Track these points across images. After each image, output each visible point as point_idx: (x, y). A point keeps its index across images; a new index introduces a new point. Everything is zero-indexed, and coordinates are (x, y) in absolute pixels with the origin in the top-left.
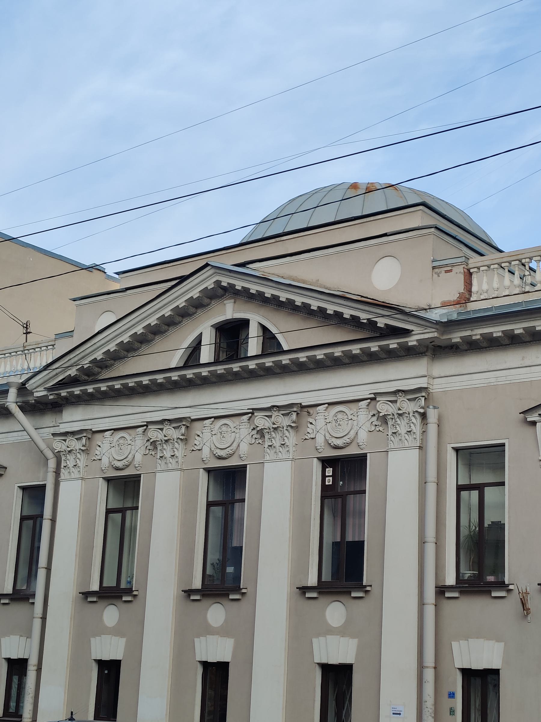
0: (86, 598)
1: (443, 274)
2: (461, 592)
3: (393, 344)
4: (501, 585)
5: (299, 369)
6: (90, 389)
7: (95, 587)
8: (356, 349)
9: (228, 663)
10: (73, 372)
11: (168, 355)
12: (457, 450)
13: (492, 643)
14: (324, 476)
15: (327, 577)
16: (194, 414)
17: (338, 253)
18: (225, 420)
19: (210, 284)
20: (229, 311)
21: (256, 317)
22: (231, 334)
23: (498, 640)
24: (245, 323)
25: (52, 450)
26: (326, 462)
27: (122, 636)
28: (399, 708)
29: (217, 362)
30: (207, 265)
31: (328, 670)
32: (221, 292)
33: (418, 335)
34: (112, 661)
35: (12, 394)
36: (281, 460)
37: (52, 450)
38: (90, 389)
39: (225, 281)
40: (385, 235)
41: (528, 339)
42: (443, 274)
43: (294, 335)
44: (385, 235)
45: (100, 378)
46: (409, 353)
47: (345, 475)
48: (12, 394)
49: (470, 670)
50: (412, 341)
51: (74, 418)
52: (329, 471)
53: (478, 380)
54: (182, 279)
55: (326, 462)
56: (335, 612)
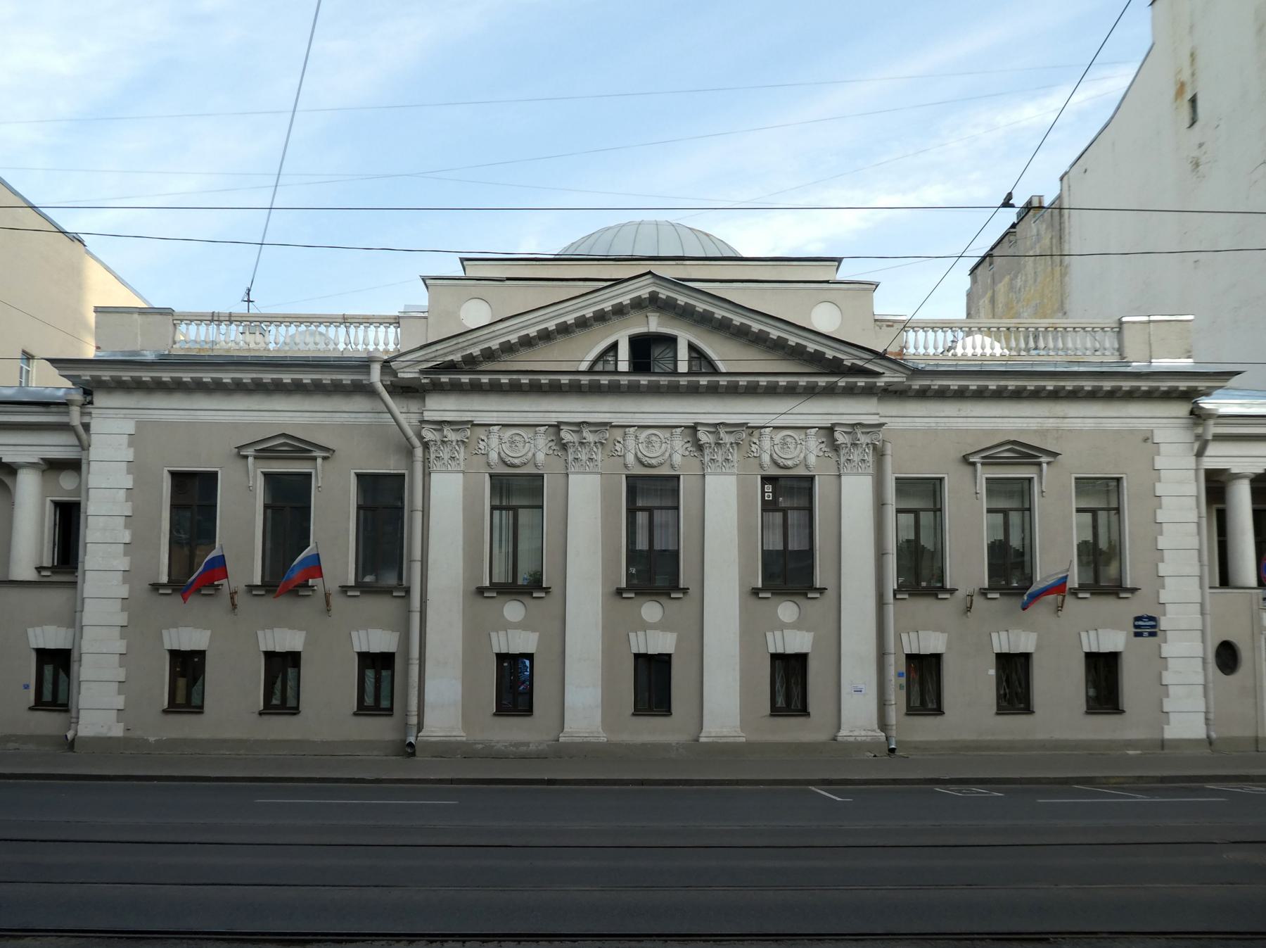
0: (250, 591)
1: (884, 328)
2: (362, 592)
3: (861, 382)
4: (943, 589)
5: (733, 391)
6: (465, 379)
7: (487, 584)
8: (803, 381)
9: (669, 656)
10: (457, 357)
11: (580, 354)
12: (358, 475)
13: (938, 634)
14: (763, 492)
15: (267, 579)
16: (754, 421)
17: (774, 289)
18: (652, 427)
19: (644, 293)
20: (654, 324)
21: (685, 336)
22: (643, 348)
23: (943, 631)
24: (671, 341)
25: (421, 438)
26: (766, 479)
27: (534, 630)
28: (860, 686)
29: (688, 374)
30: (650, 273)
31: (643, 660)
32: (653, 303)
33: (889, 377)
34: (932, 655)
35: (376, 369)
36: (725, 474)
37: (421, 438)
38: (465, 379)
39: (664, 293)
40: (827, 282)
41: (252, 387)
42: (884, 328)
43: (727, 357)
44: (827, 282)
45: (479, 369)
46: (869, 392)
47: (516, 493)
48: (376, 369)
49: (645, 656)
50: (881, 382)
51: (441, 407)
52: (768, 488)
53: (920, 423)
54: (619, 281)
55: (766, 479)
56: (651, 610)
